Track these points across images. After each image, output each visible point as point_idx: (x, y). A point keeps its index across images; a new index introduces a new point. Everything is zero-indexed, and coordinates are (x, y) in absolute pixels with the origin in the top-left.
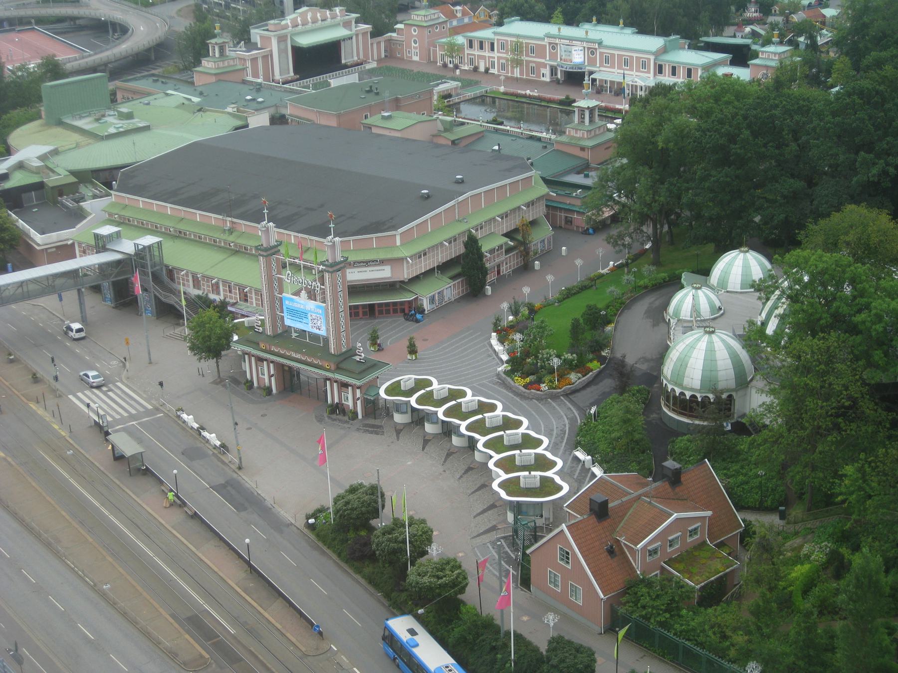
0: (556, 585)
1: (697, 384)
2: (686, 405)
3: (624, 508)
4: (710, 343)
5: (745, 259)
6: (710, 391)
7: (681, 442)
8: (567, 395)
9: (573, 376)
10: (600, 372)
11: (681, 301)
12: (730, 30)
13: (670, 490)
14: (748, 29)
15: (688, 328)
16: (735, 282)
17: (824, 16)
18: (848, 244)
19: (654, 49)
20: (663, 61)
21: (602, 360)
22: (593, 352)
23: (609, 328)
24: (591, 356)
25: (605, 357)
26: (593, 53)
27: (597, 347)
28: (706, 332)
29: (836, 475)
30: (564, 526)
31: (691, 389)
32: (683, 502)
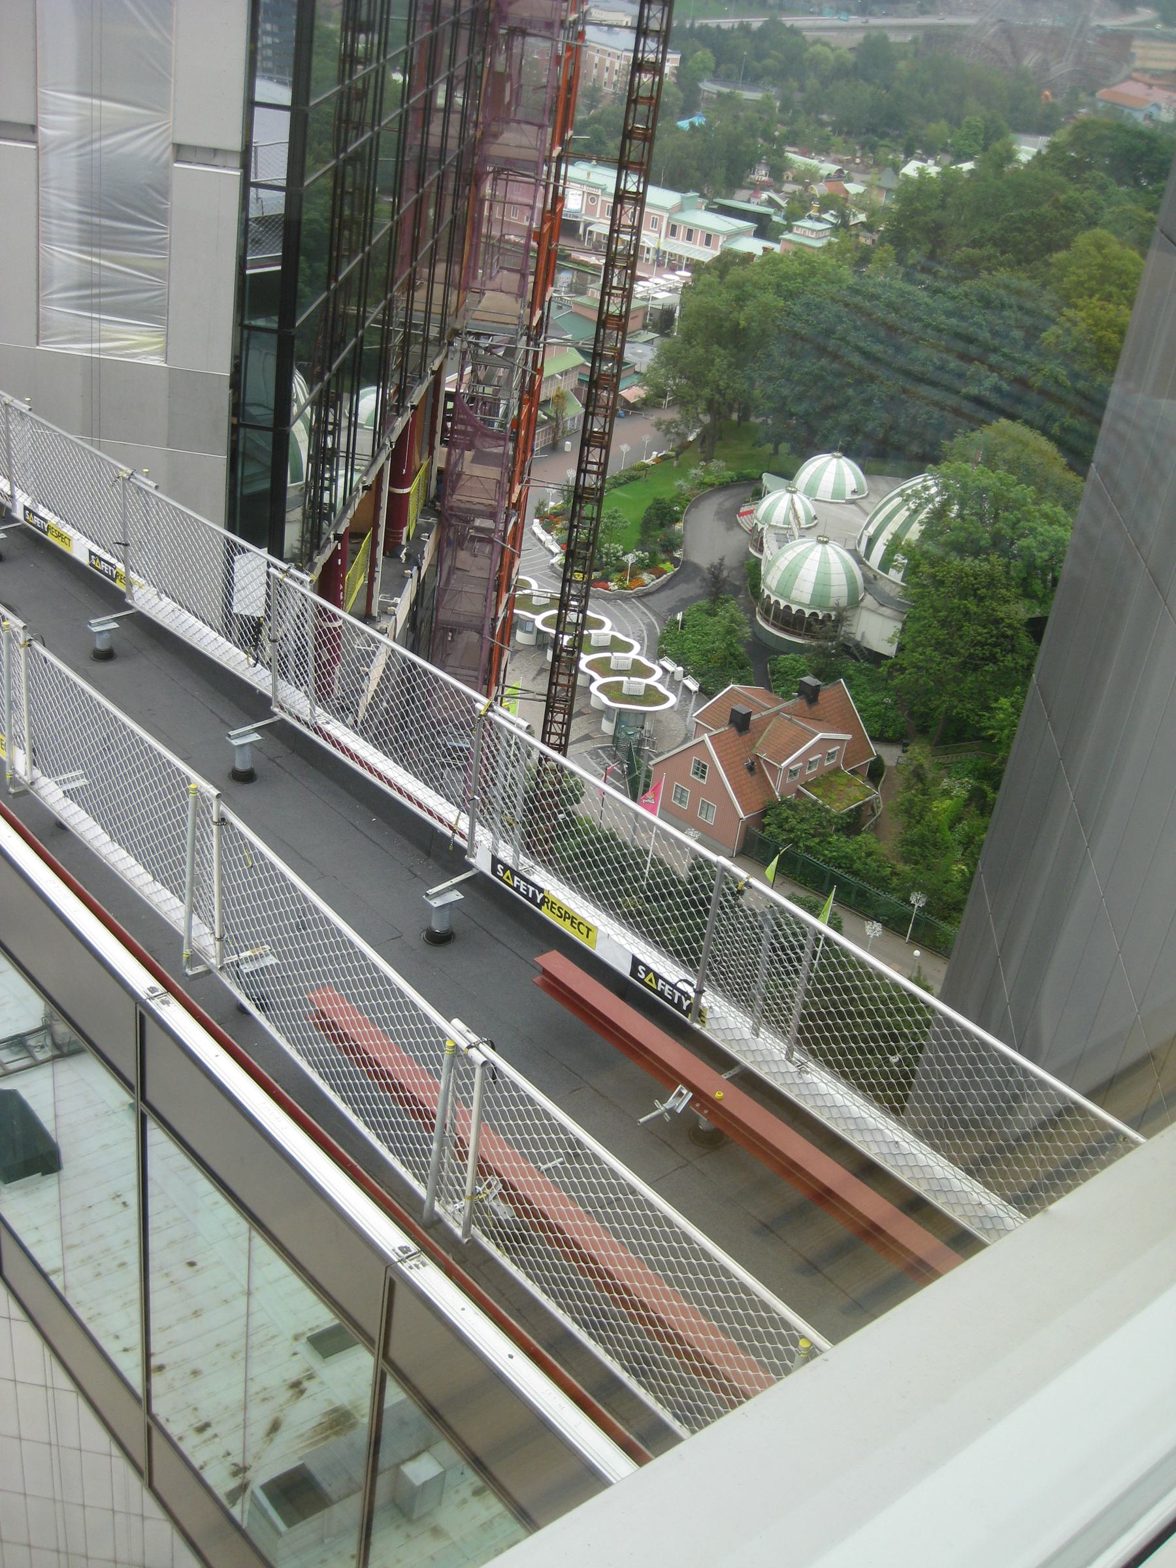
0: (681, 802)
1: (806, 598)
2: (790, 620)
3: (766, 721)
4: (825, 554)
5: (839, 467)
6: (820, 607)
7: (786, 660)
8: (639, 598)
9: (646, 577)
10: (674, 575)
11: (773, 506)
12: (743, 194)
13: (807, 708)
14: (764, 196)
16: (826, 488)
17: (847, 192)
18: (1005, 462)
19: (669, 206)
20: (678, 221)
22: (664, 552)
23: (679, 526)
24: (663, 557)
26: (593, 200)
27: (669, 546)
28: (820, 542)
29: (988, 709)
30: (706, 737)
31: (799, 603)
32: (821, 721)
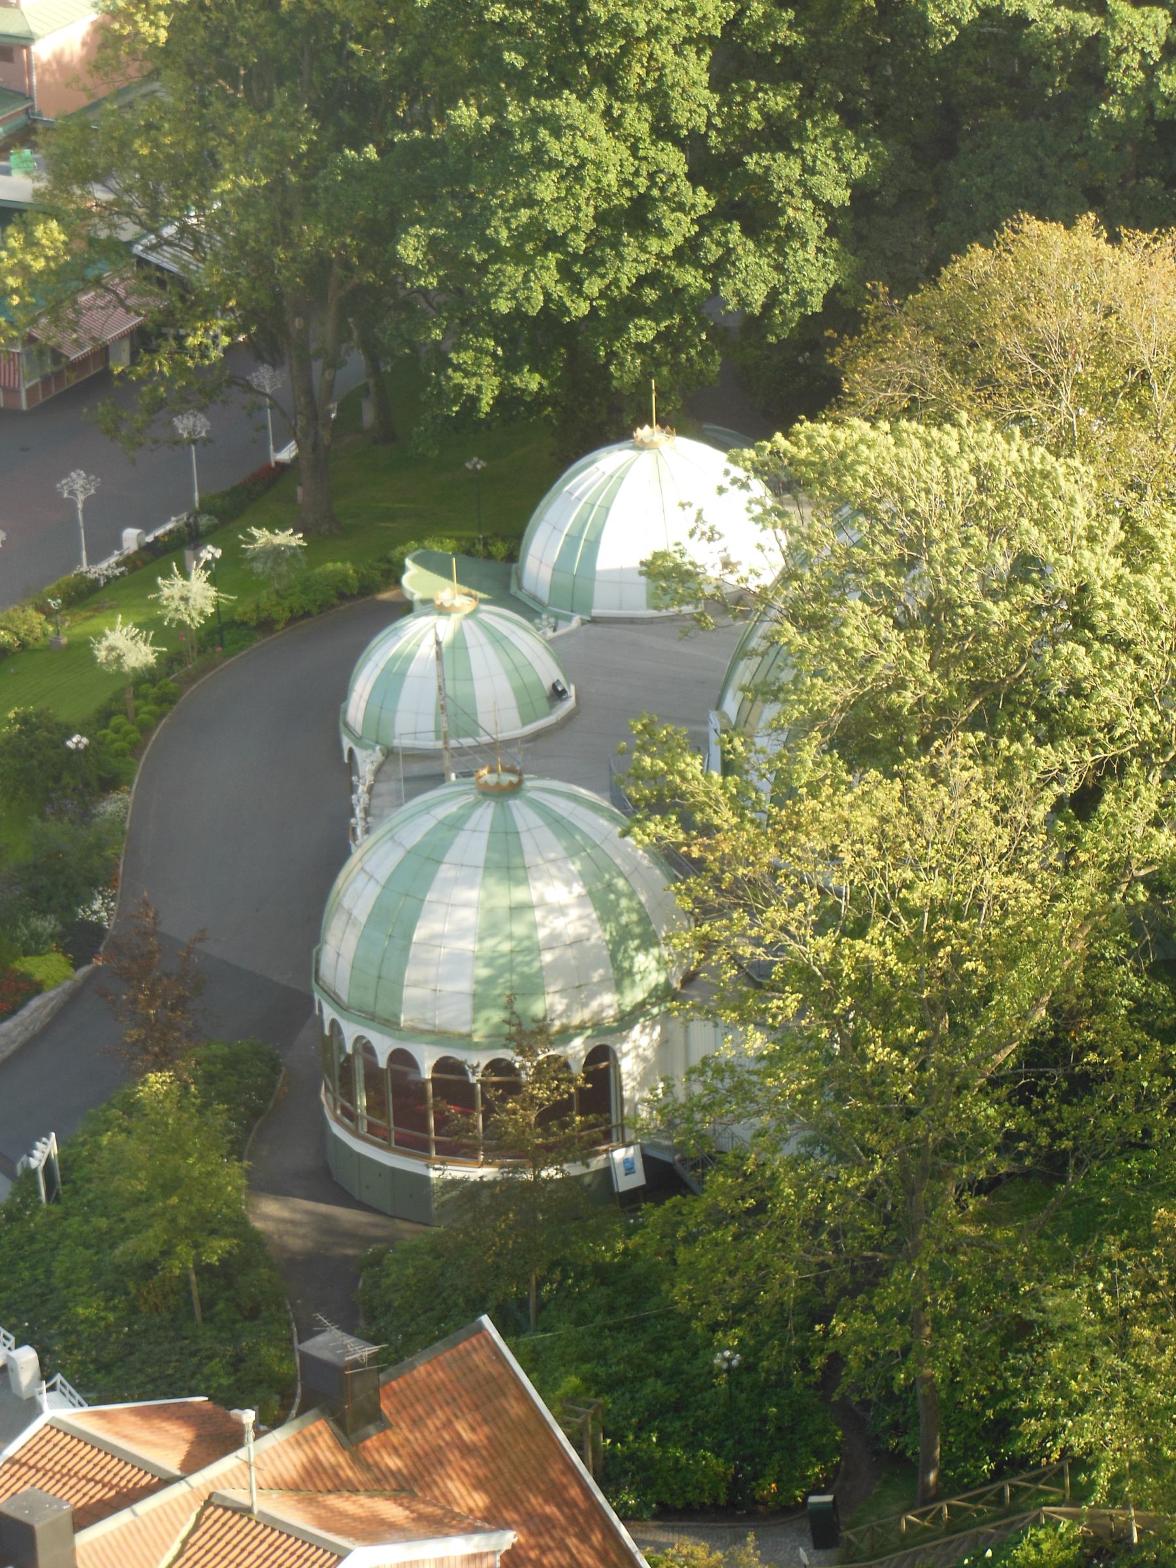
10: (74, 997)
15: (418, 772)
21: (81, 942)
23: (111, 806)
25: (95, 931)
31: (439, 1036)
